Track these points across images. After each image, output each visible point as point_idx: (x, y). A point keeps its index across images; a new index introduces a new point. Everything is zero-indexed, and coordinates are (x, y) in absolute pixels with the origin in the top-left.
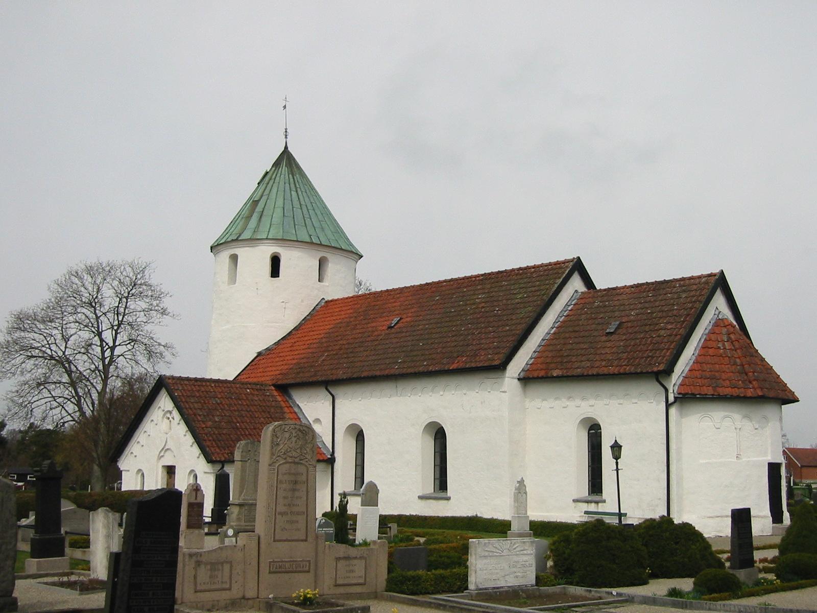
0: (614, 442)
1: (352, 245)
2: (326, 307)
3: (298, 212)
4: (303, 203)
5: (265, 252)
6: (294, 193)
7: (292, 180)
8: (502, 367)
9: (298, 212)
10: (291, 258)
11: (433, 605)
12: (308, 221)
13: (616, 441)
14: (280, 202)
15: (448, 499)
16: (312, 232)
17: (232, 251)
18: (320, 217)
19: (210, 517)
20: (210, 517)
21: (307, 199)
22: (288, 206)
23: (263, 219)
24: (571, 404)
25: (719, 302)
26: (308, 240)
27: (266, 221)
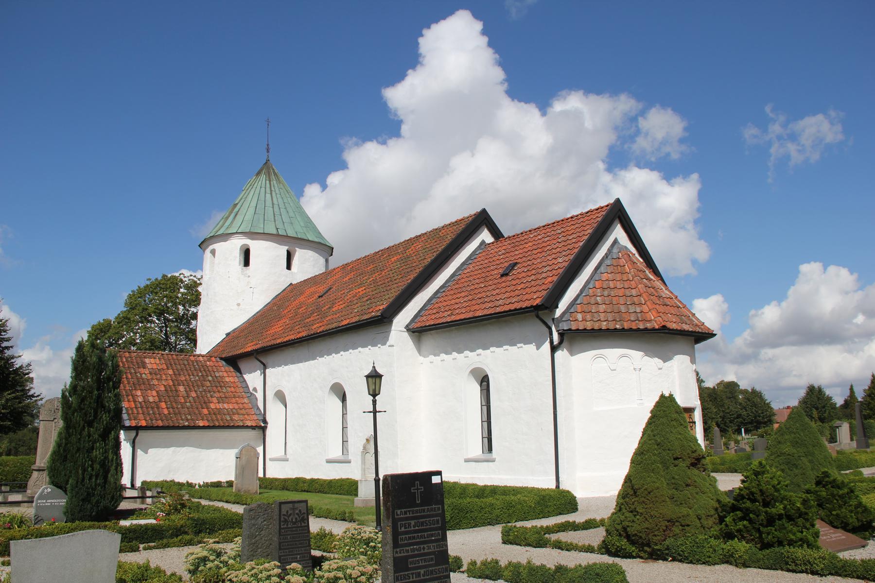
0: (371, 368)
1: (323, 238)
2: (293, 290)
3: (269, 210)
4: (275, 202)
5: (236, 244)
6: (268, 196)
7: (268, 185)
8: (384, 320)
9: (269, 210)
10: (260, 249)
11: (532, 539)
12: (278, 217)
13: (374, 367)
14: (254, 204)
15: (493, 461)
16: (280, 226)
17: (211, 247)
18: (292, 214)
19: (558, 486)
20: (558, 486)
21: (280, 200)
22: (261, 206)
23: (238, 216)
24: (460, 357)
25: (618, 233)
26: (275, 232)
27: (239, 218)
